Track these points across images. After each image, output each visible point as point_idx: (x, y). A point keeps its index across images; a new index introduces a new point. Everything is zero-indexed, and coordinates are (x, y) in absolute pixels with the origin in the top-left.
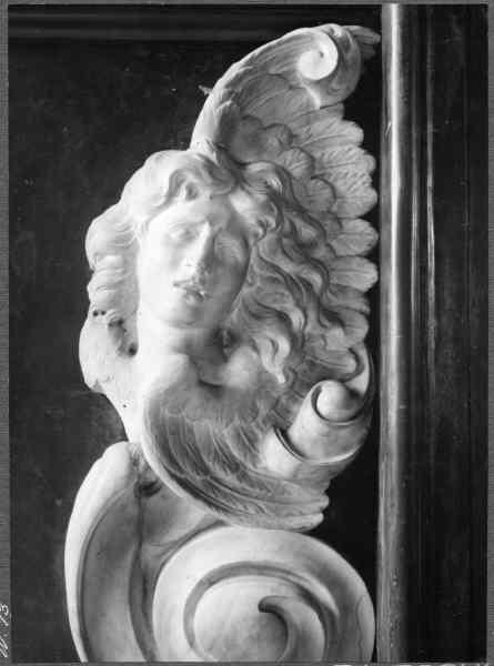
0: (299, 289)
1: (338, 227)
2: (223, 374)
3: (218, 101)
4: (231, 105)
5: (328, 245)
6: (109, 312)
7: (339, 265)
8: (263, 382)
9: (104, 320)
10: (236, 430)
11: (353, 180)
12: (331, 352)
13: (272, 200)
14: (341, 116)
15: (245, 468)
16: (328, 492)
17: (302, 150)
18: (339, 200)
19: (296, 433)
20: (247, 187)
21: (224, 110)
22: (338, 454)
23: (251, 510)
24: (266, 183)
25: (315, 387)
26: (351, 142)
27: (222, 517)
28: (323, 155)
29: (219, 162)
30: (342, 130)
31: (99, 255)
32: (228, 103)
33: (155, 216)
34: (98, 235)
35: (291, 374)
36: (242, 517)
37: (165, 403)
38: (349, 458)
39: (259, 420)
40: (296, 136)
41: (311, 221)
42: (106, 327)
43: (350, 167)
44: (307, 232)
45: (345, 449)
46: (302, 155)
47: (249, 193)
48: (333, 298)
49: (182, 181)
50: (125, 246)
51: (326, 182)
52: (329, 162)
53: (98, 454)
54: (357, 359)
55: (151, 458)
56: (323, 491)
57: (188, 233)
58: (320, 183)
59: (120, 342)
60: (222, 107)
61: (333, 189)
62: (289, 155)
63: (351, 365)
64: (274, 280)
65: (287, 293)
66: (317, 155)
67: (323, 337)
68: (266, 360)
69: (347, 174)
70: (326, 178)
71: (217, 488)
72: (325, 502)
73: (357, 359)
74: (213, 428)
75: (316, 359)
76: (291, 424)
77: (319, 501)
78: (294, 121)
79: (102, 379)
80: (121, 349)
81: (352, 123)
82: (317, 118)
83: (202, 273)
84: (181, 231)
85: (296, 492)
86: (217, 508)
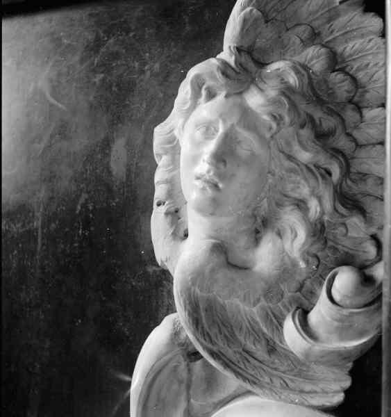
0: (317, 178)
1: (358, 116)
2: (251, 255)
3: (239, 10)
4: (251, 11)
5: (349, 135)
6: (167, 203)
7: (362, 153)
8: (286, 270)
9: (163, 209)
10: (263, 308)
11: (375, 69)
12: (350, 238)
13: (283, 94)
14: (360, 10)
15: (275, 343)
16: (352, 373)
17: (323, 46)
18: (360, 90)
19: (313, 317)
20: (261, 85)
21: (245, 15)
22: (352, 339)
23: (277, 382)
24: (283, 79)
25: (334, 270)
26: (371, 32)
27: (249, 387)
28: (345, 48)
29: (237, 66)
30: (362, 22)
31: (160, 156)
32: (248, 9)
33: (190, 114)
34: (159, 132)
35: (311, 259)
36: (270, 389)
37: (193, 284)
38: (369, 341)
39: (285, 300)
40: (319, 34)
41: (331, 112)
42: (163, 215)
43: (370, 57)
44: (328, 123)
45: (361, 334)
46: (323, 50)
47: (261, 90)
48: (354, 186)
49: (204, 84)
50: (173, 147)
51: (347, 74)
52: (351, 55)
53: (157, 323)
54: (379, 246)
55: (188, 333)
56: (347, 372)
57: (208, 129)
58: (340, 76)
59: (174, 227)
60: (242, 13)
61: (354, 79)
62: (312, 51)
63: (371, 250)
64: (291, 171)
65: (303, 181)
66: (339, 49)
67: (344, 224)
68: (287, 246)
69: (368, 65)
70: (347, 70)
71: (247, 359)
72: (347, 383)
73: (379, 246)
74: (244, 307)
75: (337, 244)
76: (314, 305)
77: (340, 381)
78: (317, 19)
79: (164, 259)
80: (174, 234)
81: (372, 14)
82: (338, 15)
83: (217, 168)
84: (203, 129)
85: (320, 370)
86: (245, 379)
